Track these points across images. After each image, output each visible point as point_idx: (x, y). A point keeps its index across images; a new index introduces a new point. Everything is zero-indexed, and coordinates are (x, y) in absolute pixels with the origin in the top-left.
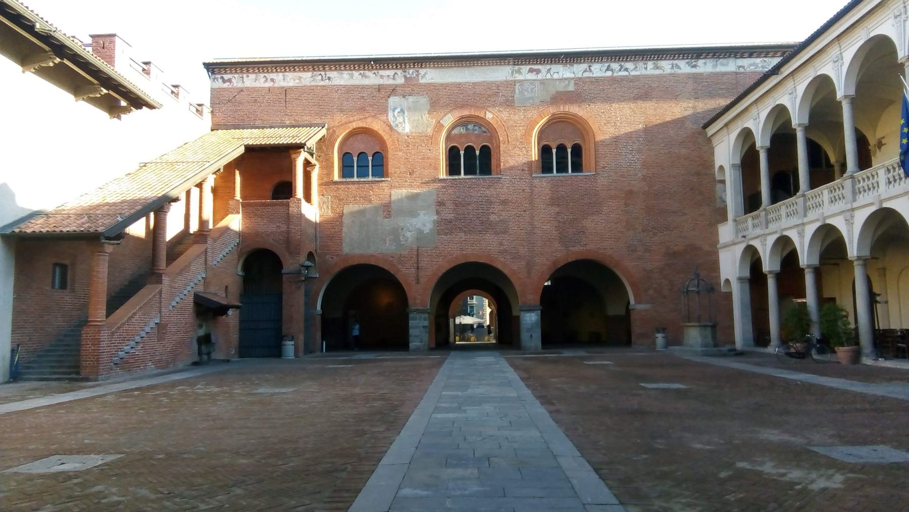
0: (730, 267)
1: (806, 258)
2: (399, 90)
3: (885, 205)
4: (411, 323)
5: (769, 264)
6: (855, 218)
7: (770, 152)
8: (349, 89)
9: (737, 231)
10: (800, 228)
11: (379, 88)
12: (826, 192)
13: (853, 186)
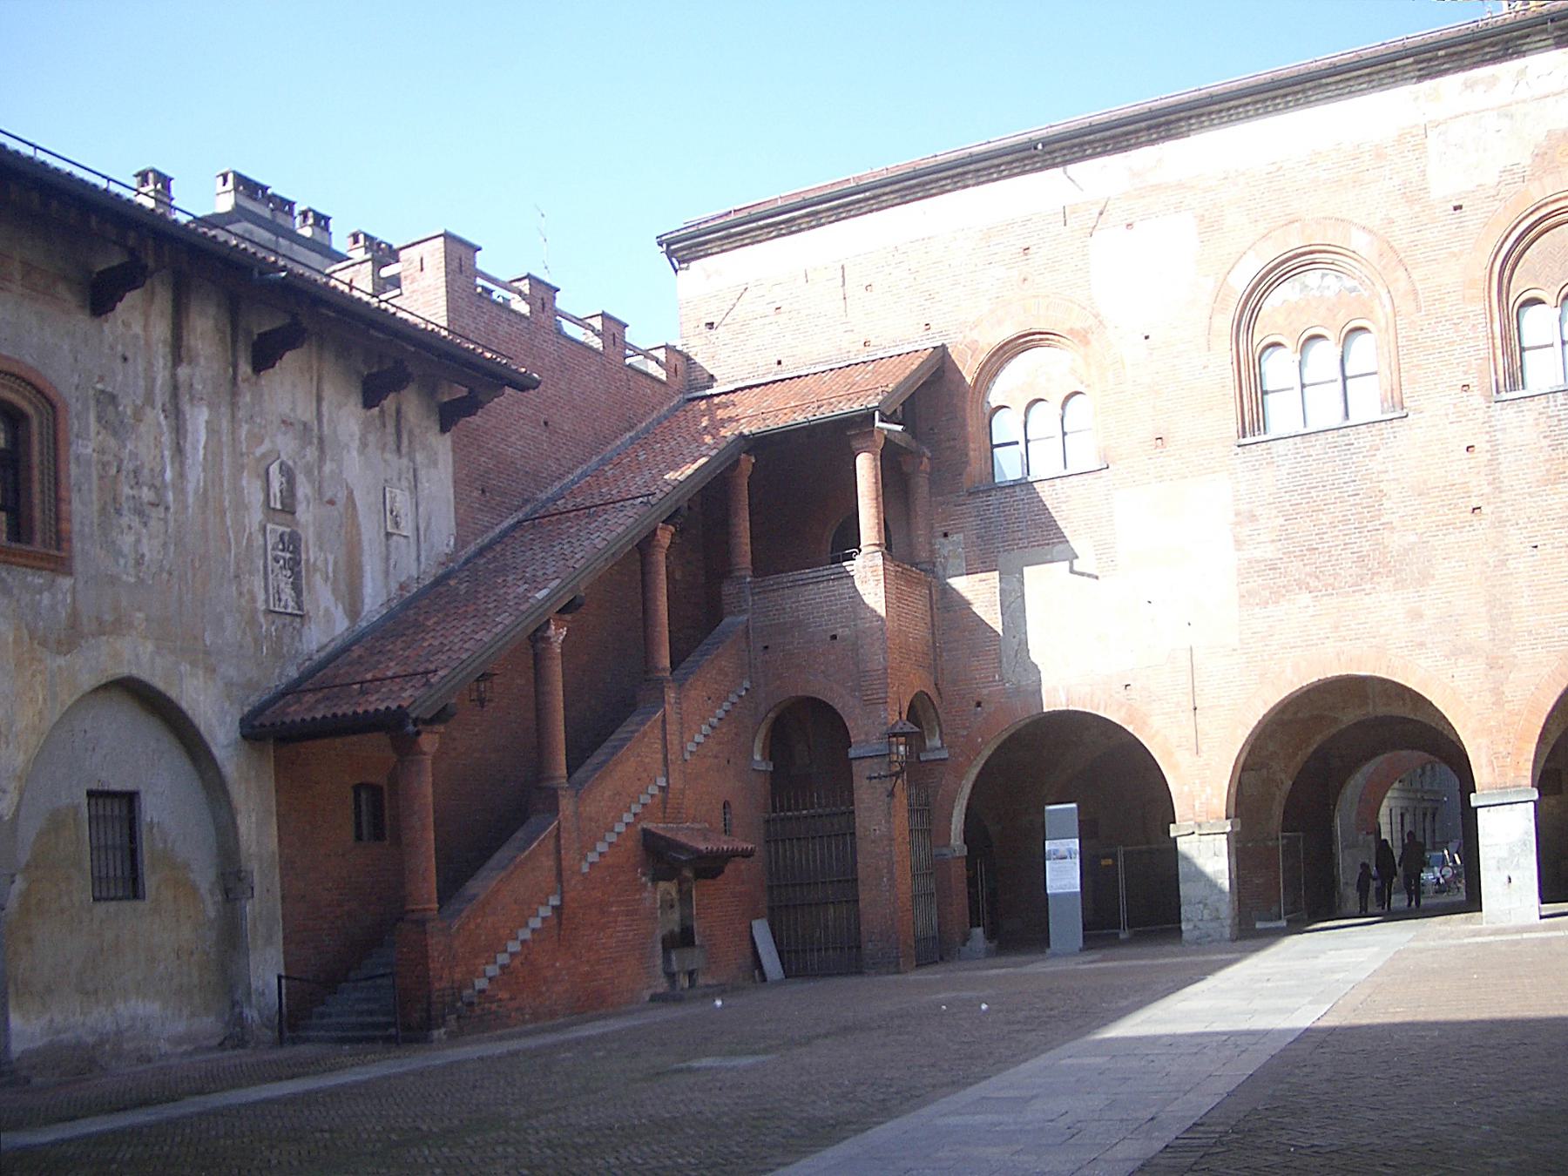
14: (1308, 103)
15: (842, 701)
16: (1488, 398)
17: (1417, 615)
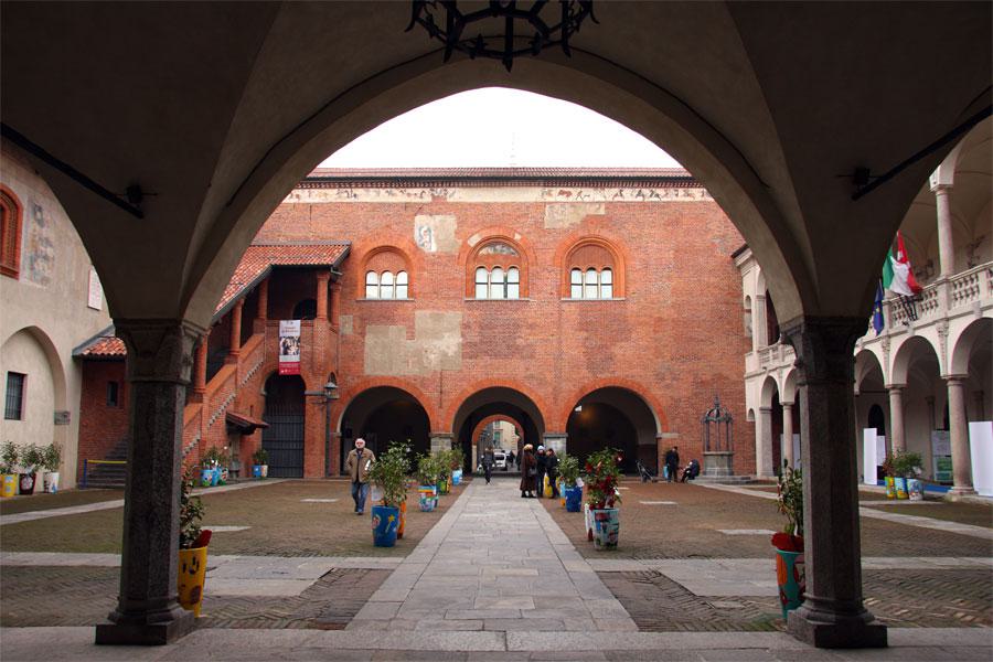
2: (426, 209)
11: (406, 206)
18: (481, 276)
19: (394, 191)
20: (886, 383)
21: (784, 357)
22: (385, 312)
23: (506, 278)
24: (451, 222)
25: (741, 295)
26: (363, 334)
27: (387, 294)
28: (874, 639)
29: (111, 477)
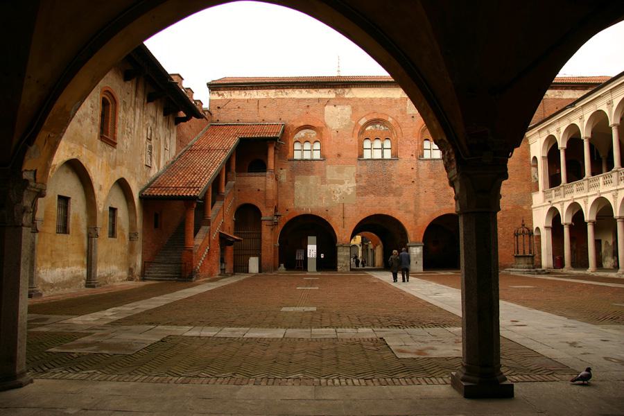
0: (540, 220)
1: (589, 216)
2: (332, 102)
3: (602, 196)
4: (339, 253)
5: (566, 219)
6: (619, 195)
7: (566, 151)
8: (299, 100)
9: (545, 198)
10: (562, 203)
11: (319, 100)
12: (601, 179)
13: (618, 176)
14: (380, 87)
15: (260, 206)
16: (417, 158)
17: (398, 203)
18: (367, 144)
19: (311, 90)
20: (615, 215)
21: (564, 195)
22: (306, 167)
23: (382, 145)
24: (348, 109)
25: (528, 156)
26: (293, 181)
27: (307, 156)
28: (507, 393)
29: (162, 273)
